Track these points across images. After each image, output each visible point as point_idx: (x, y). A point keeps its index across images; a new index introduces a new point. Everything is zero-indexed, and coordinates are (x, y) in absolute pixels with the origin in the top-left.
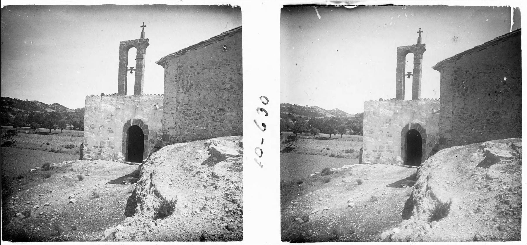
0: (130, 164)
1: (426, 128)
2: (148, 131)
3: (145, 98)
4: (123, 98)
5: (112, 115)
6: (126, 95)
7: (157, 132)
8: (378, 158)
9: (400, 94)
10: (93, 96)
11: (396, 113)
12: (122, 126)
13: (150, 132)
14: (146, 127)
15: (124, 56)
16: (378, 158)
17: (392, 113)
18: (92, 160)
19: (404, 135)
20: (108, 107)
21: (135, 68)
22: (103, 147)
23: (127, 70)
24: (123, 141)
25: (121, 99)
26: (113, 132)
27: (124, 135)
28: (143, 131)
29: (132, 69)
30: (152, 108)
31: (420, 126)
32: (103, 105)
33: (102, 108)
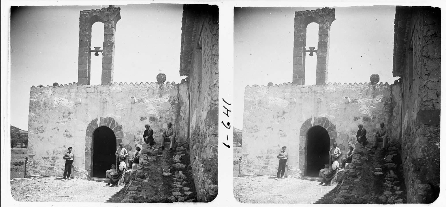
0: (97, 181)
1: (336, 124)
2: (122, 134)
3: (328, 89)
4: (85, 89)
5: (70, 113)
6: (89, 84)
7: (136, 134)
8: (51, 169)
9: (299, 76)
10: (41, 86)
11: (292, 103)
12: (85, 128)
13: (338, 134)
14: (120, 128)
15: (86, 30)
16: (51, 169)
17: (287, 102)
18: (40, 178)
19: (305, 133)
20: (278, 101)
21: (102, 48)
22: (57, 158)
23: (305, 51)
24: (87, 148)
25: (83, 91)
26: (71, 136)
27: (301, 140)
28: (329, 133)
29: (312, 51)
30: (341, 101)
31: (328, 121)
32: (56, 98)
33: (55, 102)
